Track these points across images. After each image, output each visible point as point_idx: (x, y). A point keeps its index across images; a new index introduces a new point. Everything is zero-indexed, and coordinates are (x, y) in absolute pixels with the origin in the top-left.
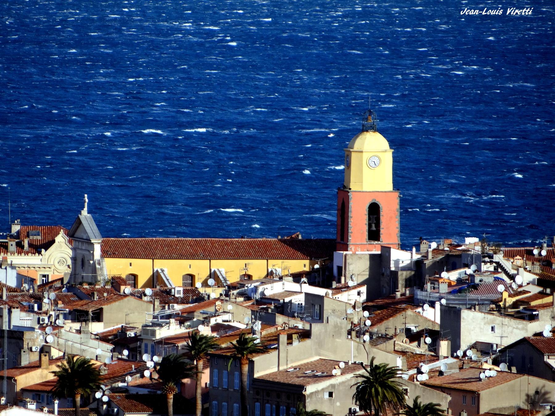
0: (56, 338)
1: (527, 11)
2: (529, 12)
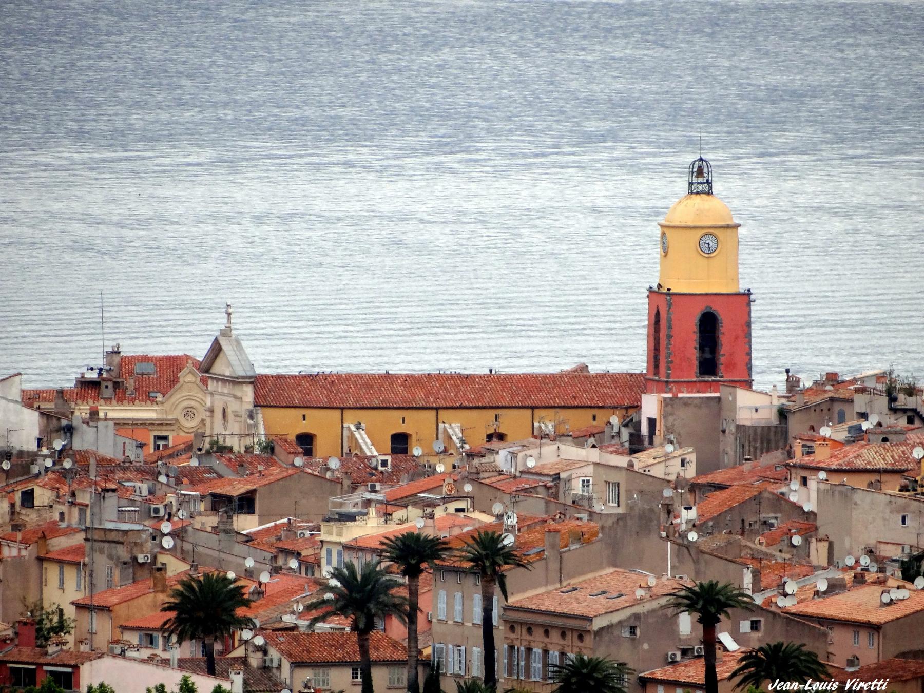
0: (178, 541)
1: (879, 684)
2: (882, 685)
